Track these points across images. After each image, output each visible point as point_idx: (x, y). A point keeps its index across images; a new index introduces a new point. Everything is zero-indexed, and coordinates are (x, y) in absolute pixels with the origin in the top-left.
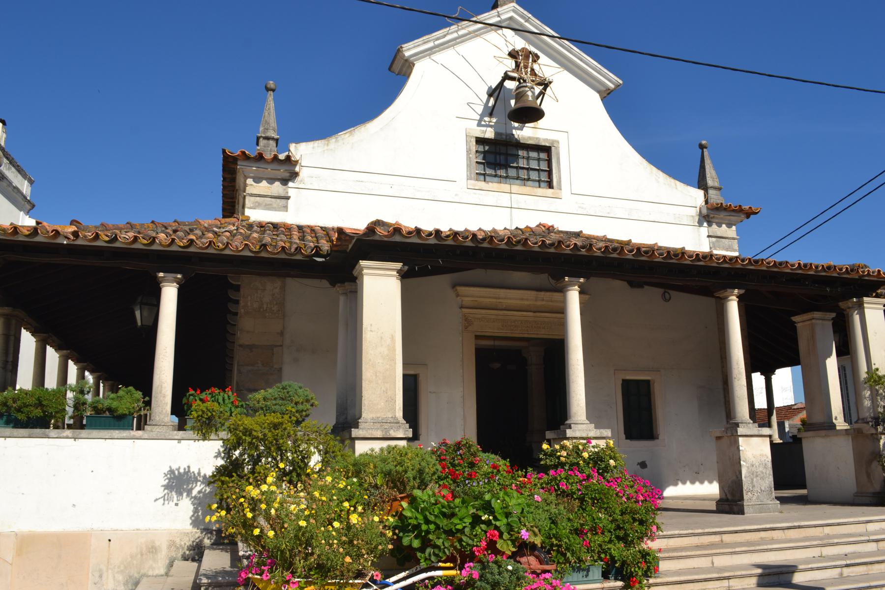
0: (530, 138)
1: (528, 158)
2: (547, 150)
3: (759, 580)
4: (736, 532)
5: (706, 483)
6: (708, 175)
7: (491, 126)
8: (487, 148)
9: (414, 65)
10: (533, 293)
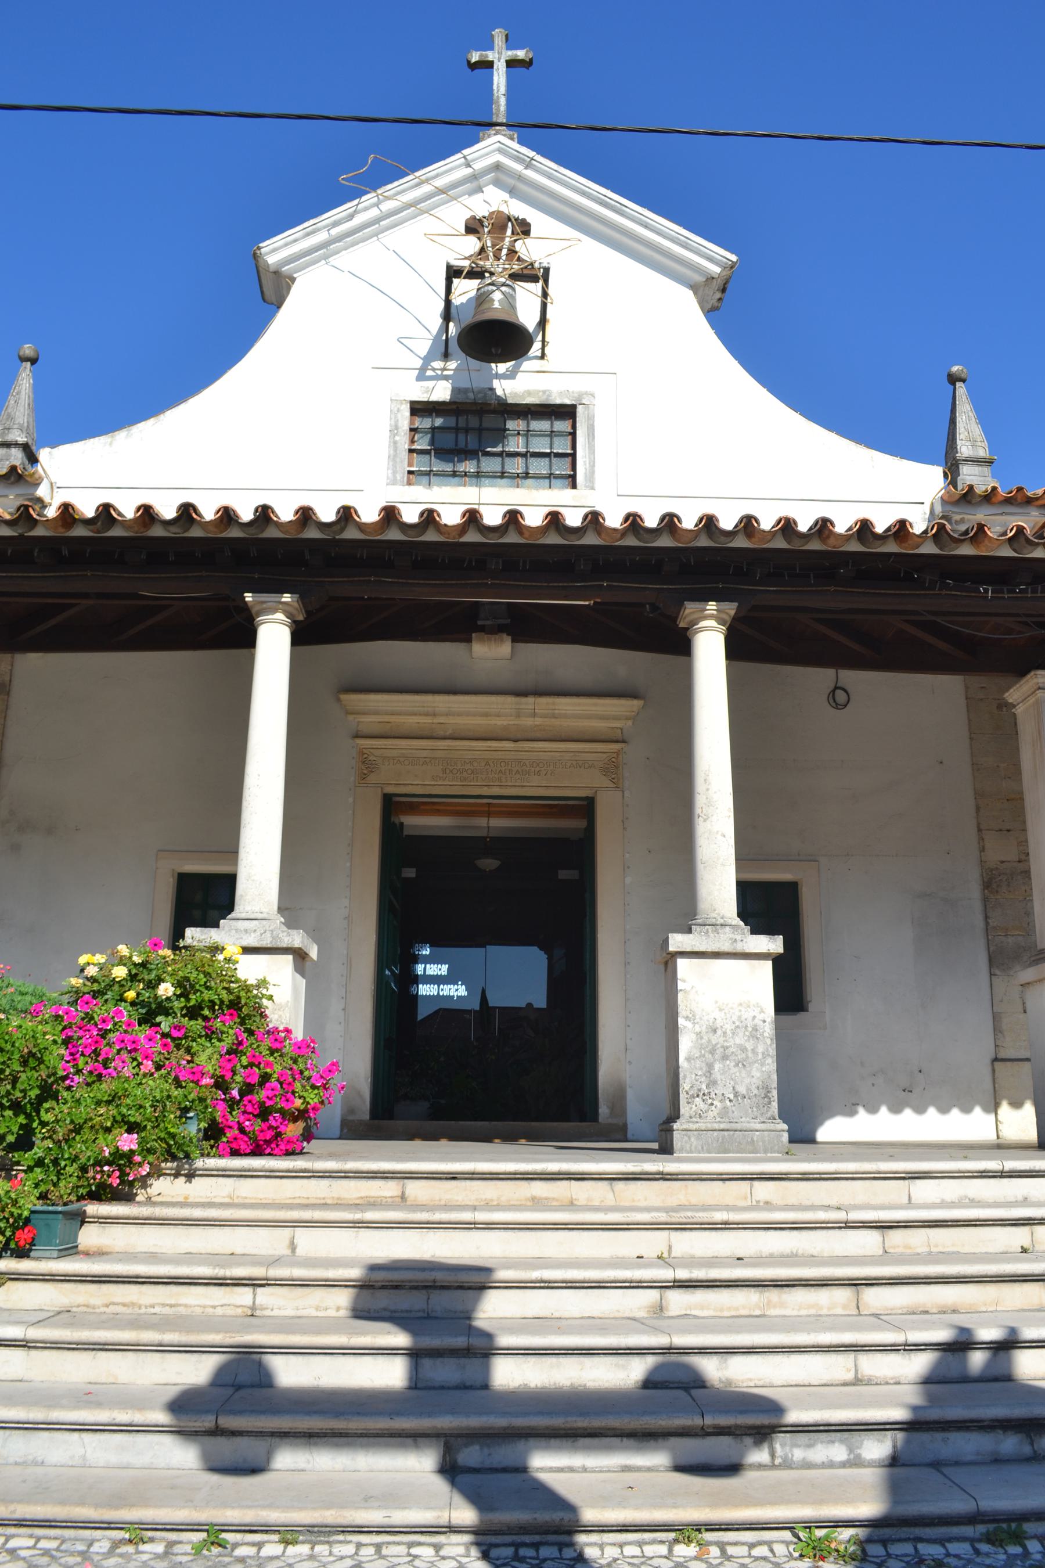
0: (529, 393)
1: (528, 433)
2: (567, 412)
3: (357, 1299)
4: (453, 1177)
5: (932, 1111)
6: (961, 434)
7: (446, 378)
8: (439, 422)
9: (293, 280)
10: (509, 702)
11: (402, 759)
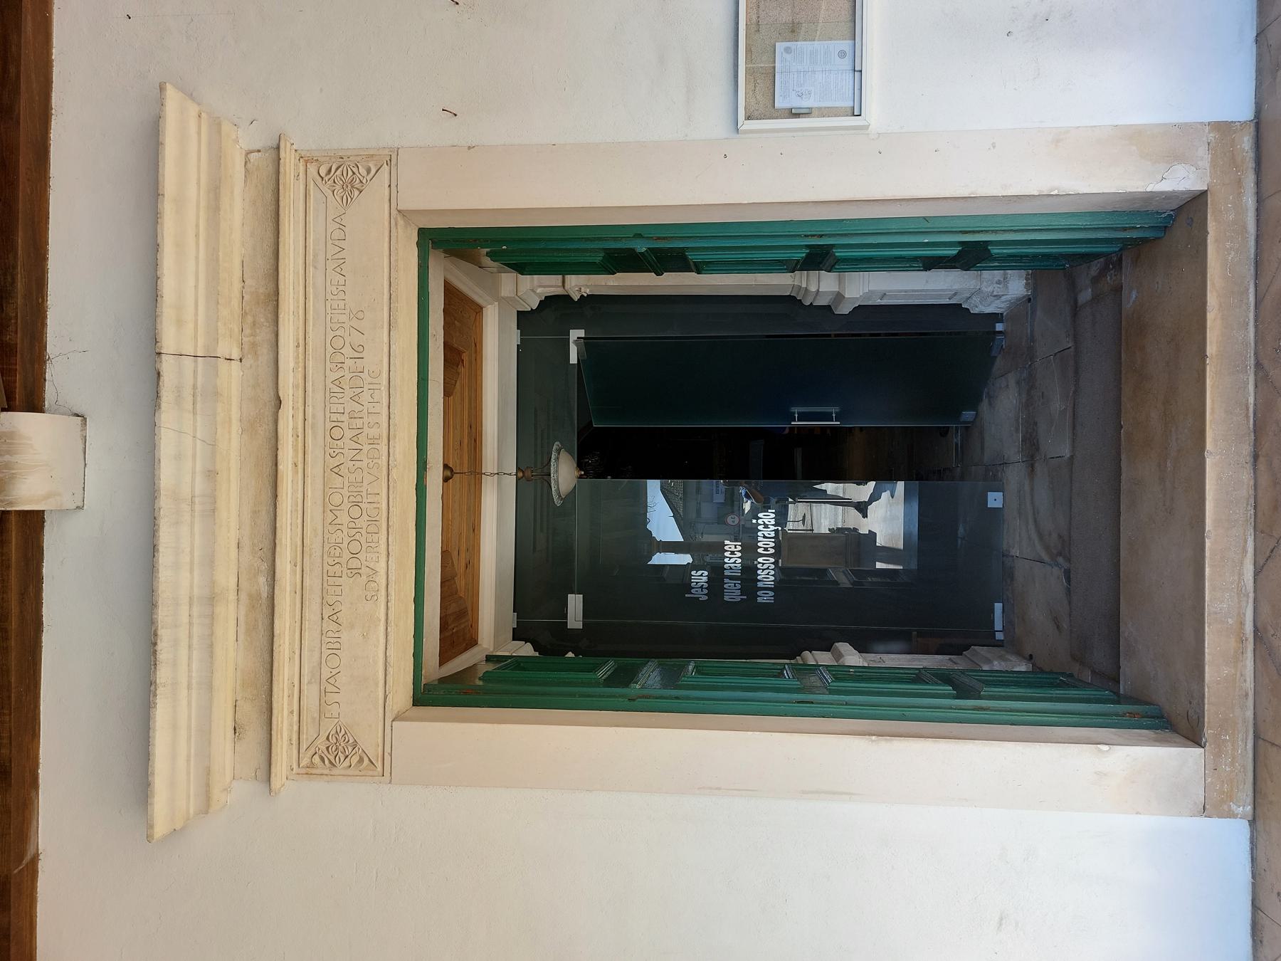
11: (326, 673)
